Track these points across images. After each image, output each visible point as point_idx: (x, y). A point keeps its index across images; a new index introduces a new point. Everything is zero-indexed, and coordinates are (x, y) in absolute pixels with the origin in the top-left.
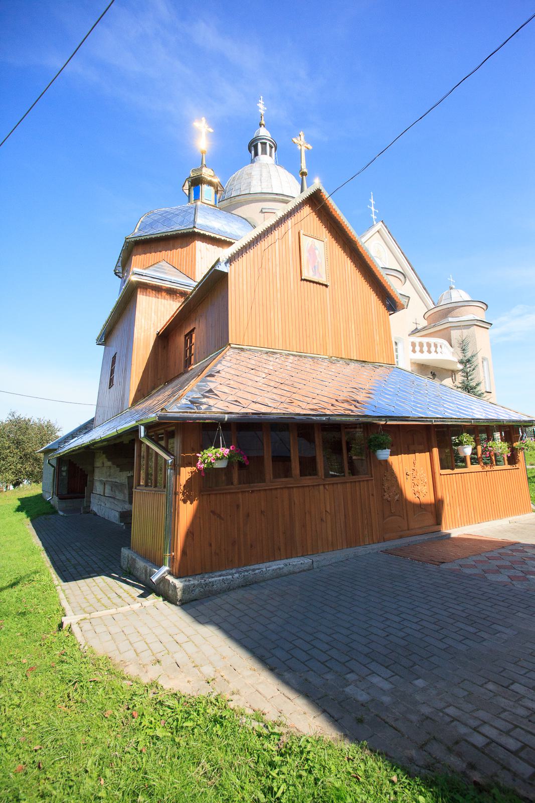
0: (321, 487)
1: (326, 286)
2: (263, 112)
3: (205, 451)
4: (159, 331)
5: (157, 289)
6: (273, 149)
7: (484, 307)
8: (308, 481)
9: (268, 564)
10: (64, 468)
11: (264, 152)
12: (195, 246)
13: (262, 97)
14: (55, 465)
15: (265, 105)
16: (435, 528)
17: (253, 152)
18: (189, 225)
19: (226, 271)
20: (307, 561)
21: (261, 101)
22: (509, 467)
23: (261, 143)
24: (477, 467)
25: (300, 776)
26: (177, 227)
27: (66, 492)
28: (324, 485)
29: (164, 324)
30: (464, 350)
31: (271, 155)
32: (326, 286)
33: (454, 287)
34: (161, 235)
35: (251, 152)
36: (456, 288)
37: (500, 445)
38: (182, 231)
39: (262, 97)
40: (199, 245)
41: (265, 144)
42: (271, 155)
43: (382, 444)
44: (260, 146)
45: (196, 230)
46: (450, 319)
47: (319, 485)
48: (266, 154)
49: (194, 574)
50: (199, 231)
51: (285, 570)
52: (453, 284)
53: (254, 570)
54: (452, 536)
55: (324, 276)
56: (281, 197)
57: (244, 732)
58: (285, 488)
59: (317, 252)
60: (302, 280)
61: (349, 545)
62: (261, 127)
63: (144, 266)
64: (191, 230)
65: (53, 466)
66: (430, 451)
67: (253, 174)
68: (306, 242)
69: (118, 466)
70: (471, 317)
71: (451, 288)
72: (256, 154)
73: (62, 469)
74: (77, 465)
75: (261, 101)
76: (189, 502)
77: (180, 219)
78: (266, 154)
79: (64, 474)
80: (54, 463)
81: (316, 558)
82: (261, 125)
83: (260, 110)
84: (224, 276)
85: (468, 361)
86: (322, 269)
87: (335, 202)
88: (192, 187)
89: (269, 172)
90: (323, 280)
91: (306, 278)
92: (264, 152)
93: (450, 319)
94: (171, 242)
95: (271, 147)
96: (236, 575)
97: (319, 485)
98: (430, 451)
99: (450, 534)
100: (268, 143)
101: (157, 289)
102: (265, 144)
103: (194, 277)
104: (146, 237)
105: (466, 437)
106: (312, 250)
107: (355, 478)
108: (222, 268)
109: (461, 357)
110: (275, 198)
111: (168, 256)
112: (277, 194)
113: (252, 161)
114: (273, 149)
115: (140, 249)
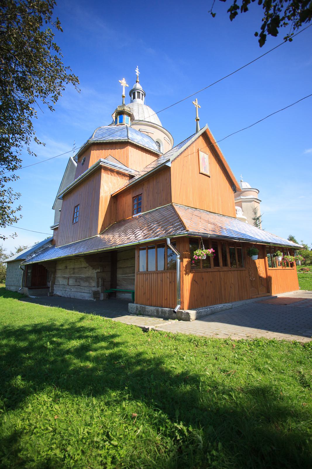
0: (230, 272)
1: (209, 177)
2: (138, 75)
3: (90, 266)
4: (112, 194)
5: (112, 171)
6: (144, 96)
7: (258, 192)
8: (225, 269)
9: (218, 305)
10: (29, 271)
11: (139, 97)
12: (128, 149)
13: (138, 66)
14: (24, 269)
15: (139, 71)
16: (268, 294)
17: (132, 96)
18: (125, 137)
19: (170, 166)
20: (230, 304)
21: (137, 69)
22: (291, 268)
23: (137, 92)
24: (280, 267)
25: (305, 357)
26: (123, 139)
27: (30, 285)
28: (231, 271)
29: (117, 191)
30: (256, 213)
31: (142, 99)
32: (209, 177)
33: (242, 180)
34: (109, 141)
35: (131, 96)
36: (244, 182)
37: (290, 257)
38: (122, 140)
39: (138, 66)
40: (130, 148)
41: (140, 92)
42: (142, 99)
43: (255, 253)
44: (136, 94)
45: (130, 141)
46: (242, 197)
47: (229, 271)
48: (140, 98)
49: (206, 305)
50: (131, 141)
51: (224, 308)
52: (243, 179)
53: (214, 307)
54: (278, 297)
55: (208, 172)
56: (150, 124)
57: (204, 387)
58: (219, 271)
59: (205, 159)
60: (200, 173)
61: (240, 300)
62: (137, 83)
63: (104, 157)
64: (127, 140)
65: (23, 270)
66: (264, 258)
67: (134, 109)
68: (201, 154)
69: (91, 266)
70: (251, 197)
71: (241, 181)
72: (134, 98)
73: (28, 271)
74: (46, 268)
75: (137, 69)
76: (187, 275)
77: (119, 133)
78: (140, 98)
79: (29, 274)
80: (23, 268)
81: (234, 303)
82: (137, 82)
83: (136, 74)
84: (169, 168)
85: (258, 219)
86: (208, 168)
87: (214, 136)
88: (118, 116)
89: (143, 109)
90: (208, 174)
91: (202, 172)
92: (139, 97)
93: (242, 197)
94: (114, 146)
95: (142, 95)
96: (209, 309)
97: (229, 271)
98: (264, 258)
99: (277, 296)
100: (141, 92)
101: (112, 171)
102: (140, 92)
103: (128, 166)
104: (100, 141)
105: (279, 252)
106: (204, 159)
107: (241, 269)
108: (169, 164)
109: (253, 217)
110: (147, 124)
111: (112, 152)
112: (148, 122)
113: (132, 102)
114: (144, 96)
115: (96, 147)
